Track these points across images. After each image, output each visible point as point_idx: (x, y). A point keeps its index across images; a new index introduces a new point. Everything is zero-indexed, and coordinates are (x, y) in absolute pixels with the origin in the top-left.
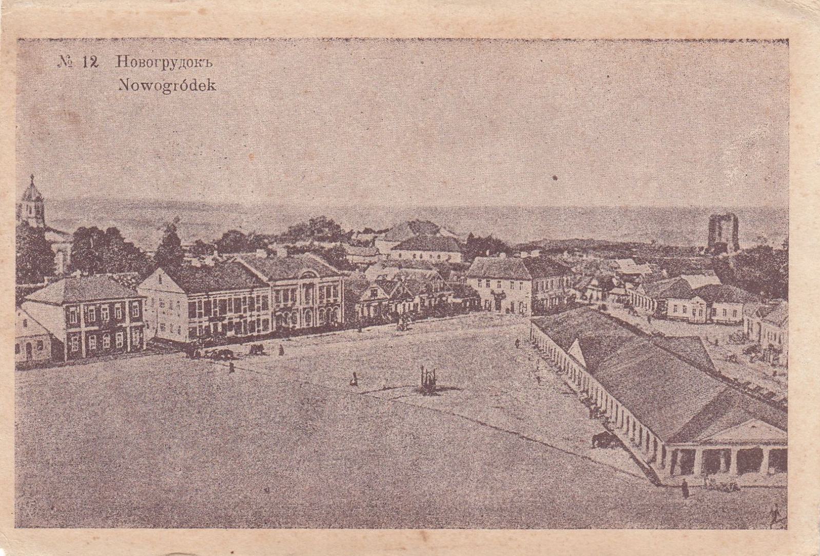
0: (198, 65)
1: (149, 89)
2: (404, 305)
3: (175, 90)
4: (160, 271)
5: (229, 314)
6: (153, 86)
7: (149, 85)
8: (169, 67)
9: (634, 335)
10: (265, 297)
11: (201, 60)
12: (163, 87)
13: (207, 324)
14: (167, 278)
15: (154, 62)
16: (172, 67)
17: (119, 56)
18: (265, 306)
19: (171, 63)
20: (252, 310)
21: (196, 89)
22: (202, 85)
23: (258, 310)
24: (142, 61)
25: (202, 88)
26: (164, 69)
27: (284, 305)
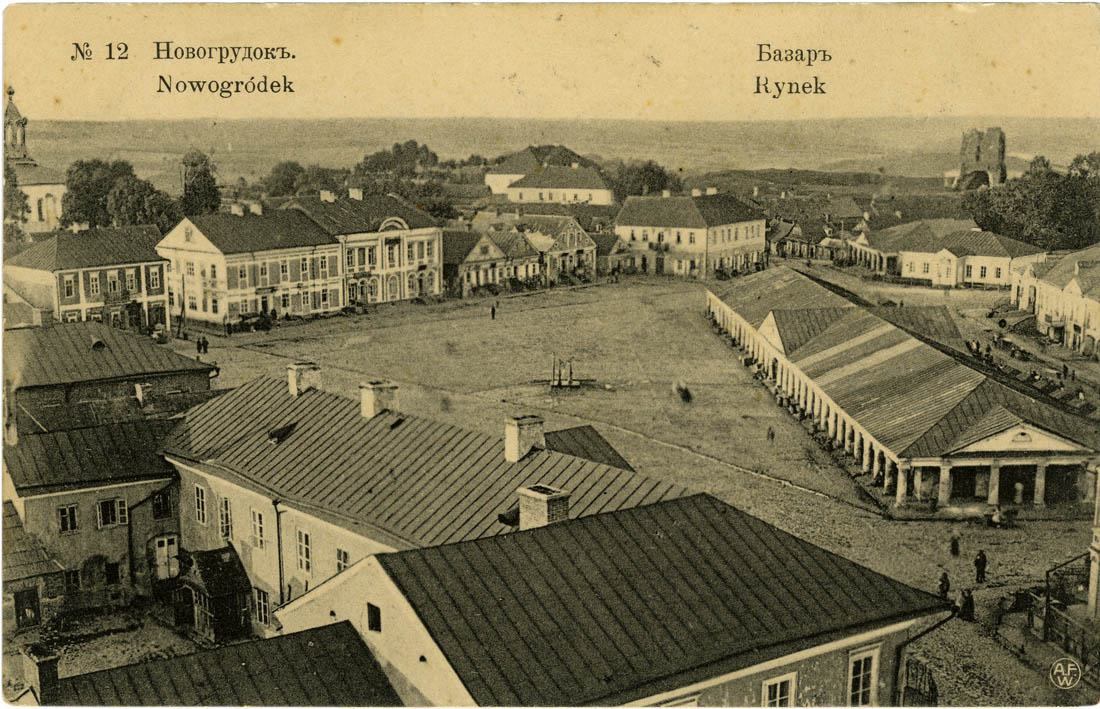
0: (269, 56)
1: (201, 90)
2: (527, 266)
3: (237, 91)
4: (186, 223)
5: (284, 284)
6: (206, 85)
7: (201, 84)
8: (229, 59)
9: (855, 306)
10: (334, 260)
11: (273, 49)
12: (220, 87)
13: (253, 297)
14: (198, 235)
15: (208, 51)
16: (233, 57)
17: (158, 44)
18: (334, 273)
19: (231, 51)
20: (313, 277)
21: (265, 90)
22: (275, 84)
23: (325, 277)
24: (191, 50)
25: (275, 89)
26: (221, 62)
27: (360, 269)
